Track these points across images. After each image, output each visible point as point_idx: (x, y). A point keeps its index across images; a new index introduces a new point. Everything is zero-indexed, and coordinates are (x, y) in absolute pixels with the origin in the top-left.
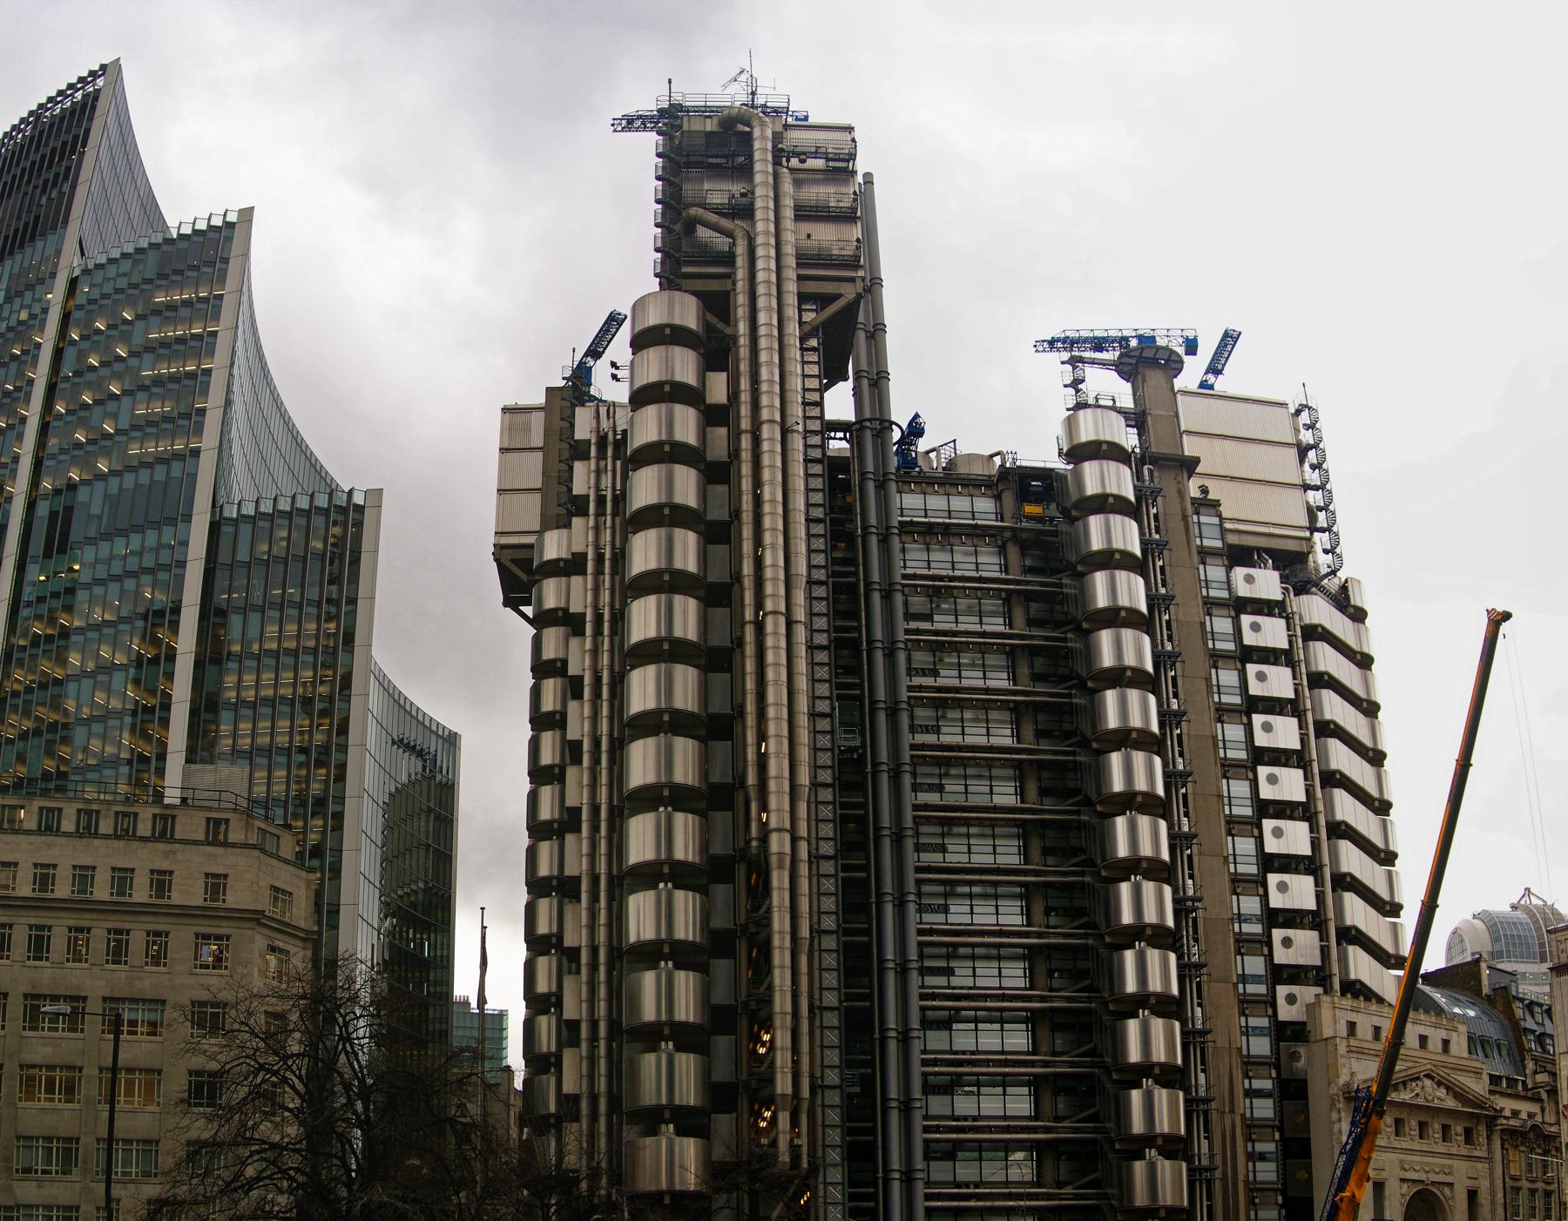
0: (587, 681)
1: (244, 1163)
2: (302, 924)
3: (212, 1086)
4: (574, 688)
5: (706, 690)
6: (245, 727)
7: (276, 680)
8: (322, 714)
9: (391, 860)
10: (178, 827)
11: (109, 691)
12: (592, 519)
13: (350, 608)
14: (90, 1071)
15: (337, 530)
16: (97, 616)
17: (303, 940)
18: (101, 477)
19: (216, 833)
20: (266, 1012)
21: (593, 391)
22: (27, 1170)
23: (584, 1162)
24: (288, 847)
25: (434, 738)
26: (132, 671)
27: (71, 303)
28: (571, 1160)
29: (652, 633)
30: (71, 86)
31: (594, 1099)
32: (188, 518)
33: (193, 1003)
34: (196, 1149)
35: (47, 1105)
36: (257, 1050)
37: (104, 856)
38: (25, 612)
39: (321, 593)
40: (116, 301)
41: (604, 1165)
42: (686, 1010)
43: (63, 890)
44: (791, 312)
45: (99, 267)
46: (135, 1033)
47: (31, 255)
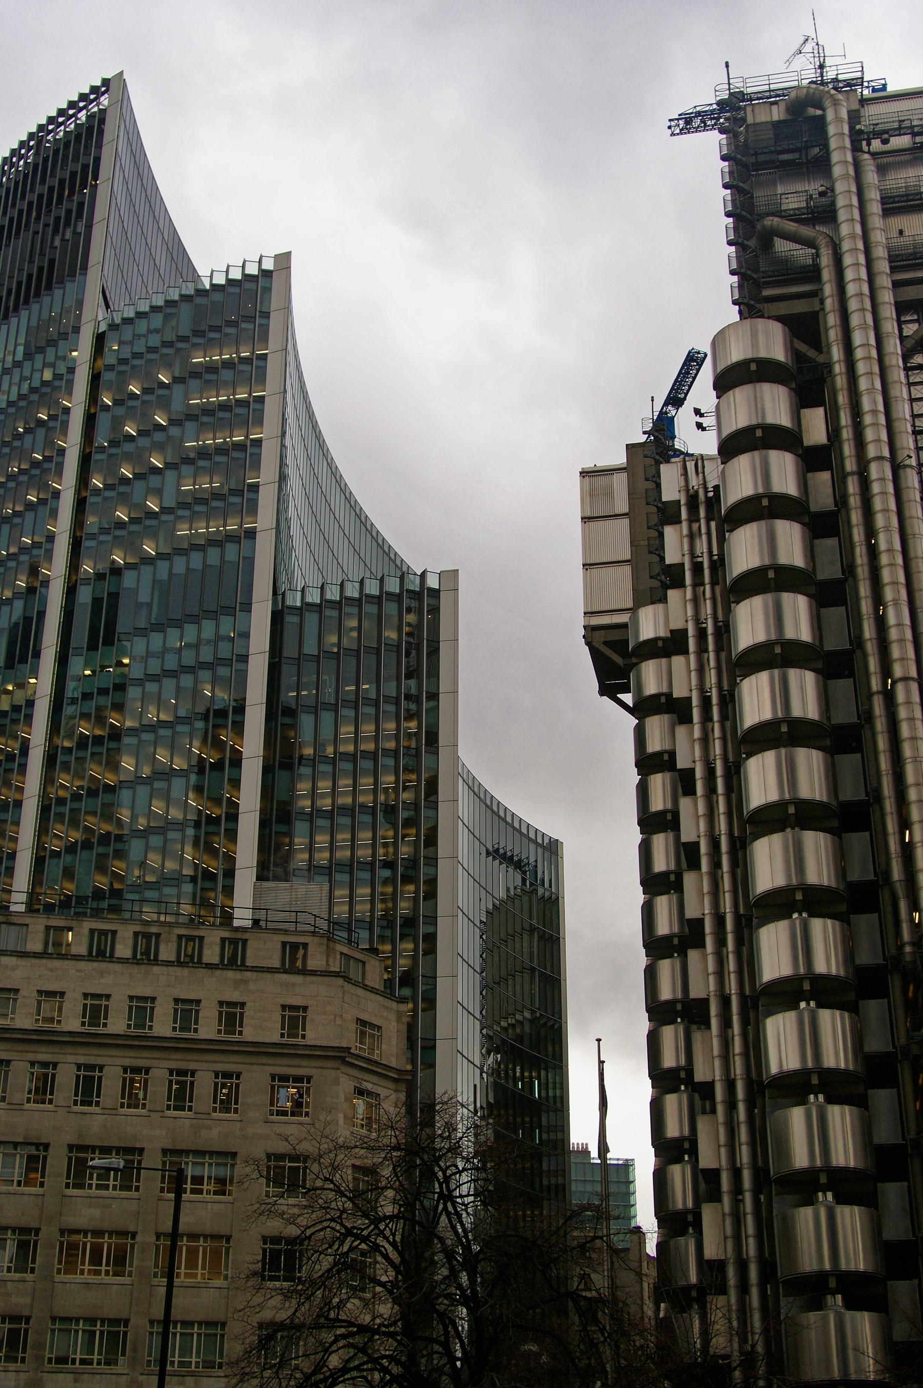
0: (699, 774)
1: (327, 1351)
2: (393, 1063)
3: (290, 1255)
4: (685, 783)
5: (834, 775)
6: (322, 839)
7: (355, 786)
8: (408, 823)
9: (492, 986)
10: (249, 952)
11: (168, 799)
12: (689, 590)
13: (432, 704)
14: (146, 1237)
15: (411, 618)
16: (151, 715)
17: (395, 1080)
18: (148, 560)
19: (293, 960)
20: (354, 1166)
22: (62, 1360)
23: (736, 1345)
24: (375, 974)
25: (532, 846)
26: (193, 778)
27: (100, 363)
28: (719, 1343)
29: (767, 715)
30: (72, 104)
31: (742, 1266)
32: (247, 607)
33: (269, 1156)
34: (270, 1334)
35: (92, 1279)
36: (344, 1211)
37: (165, 985)
38: (68, 710)
39: (399, 688)
40: (149, 361)
41: (760, 1349)
42: (845, 1152)
43: (117, 1023)
44: (890, 327)
45: (127, 321)
46: (200, 1192)
47: (51, 304)
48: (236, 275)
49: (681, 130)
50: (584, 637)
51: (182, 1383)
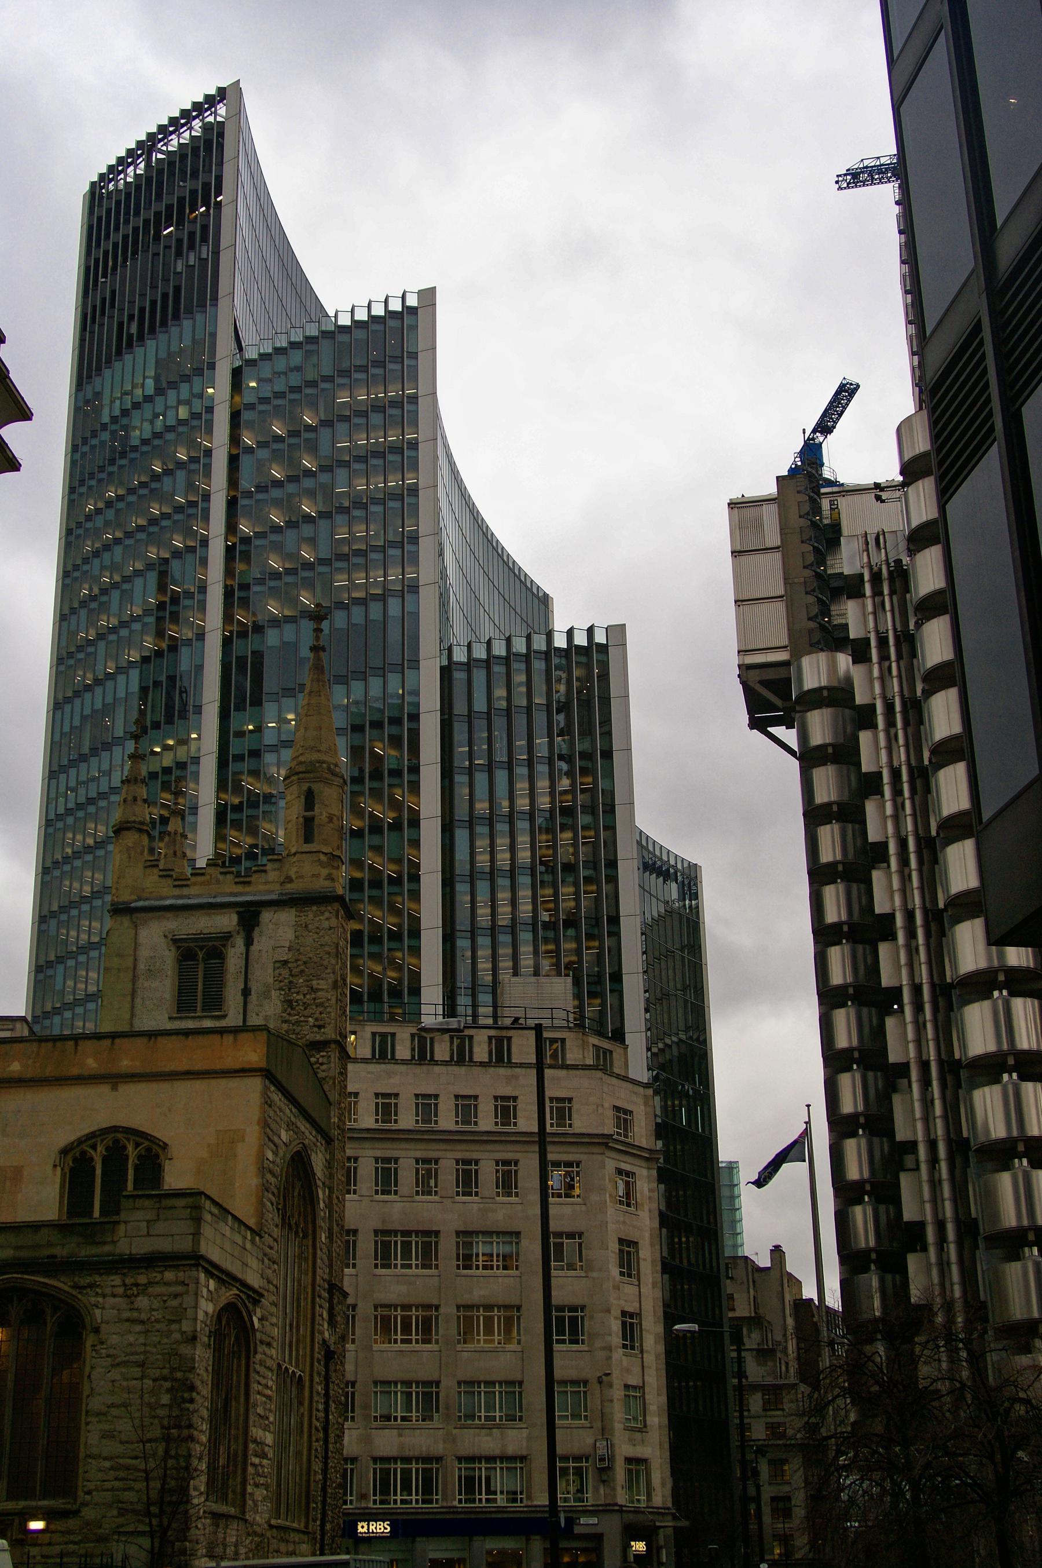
10: (514, 1049)
17: (647, 1159)
21: (827, 474)
32: (415, 664)
37: (446, 1082)
43: (407, 1119)
47: (181, 335)
48: (378, 310)
49: (848, 184)
50: (739, 676)
51: (491, 1435)
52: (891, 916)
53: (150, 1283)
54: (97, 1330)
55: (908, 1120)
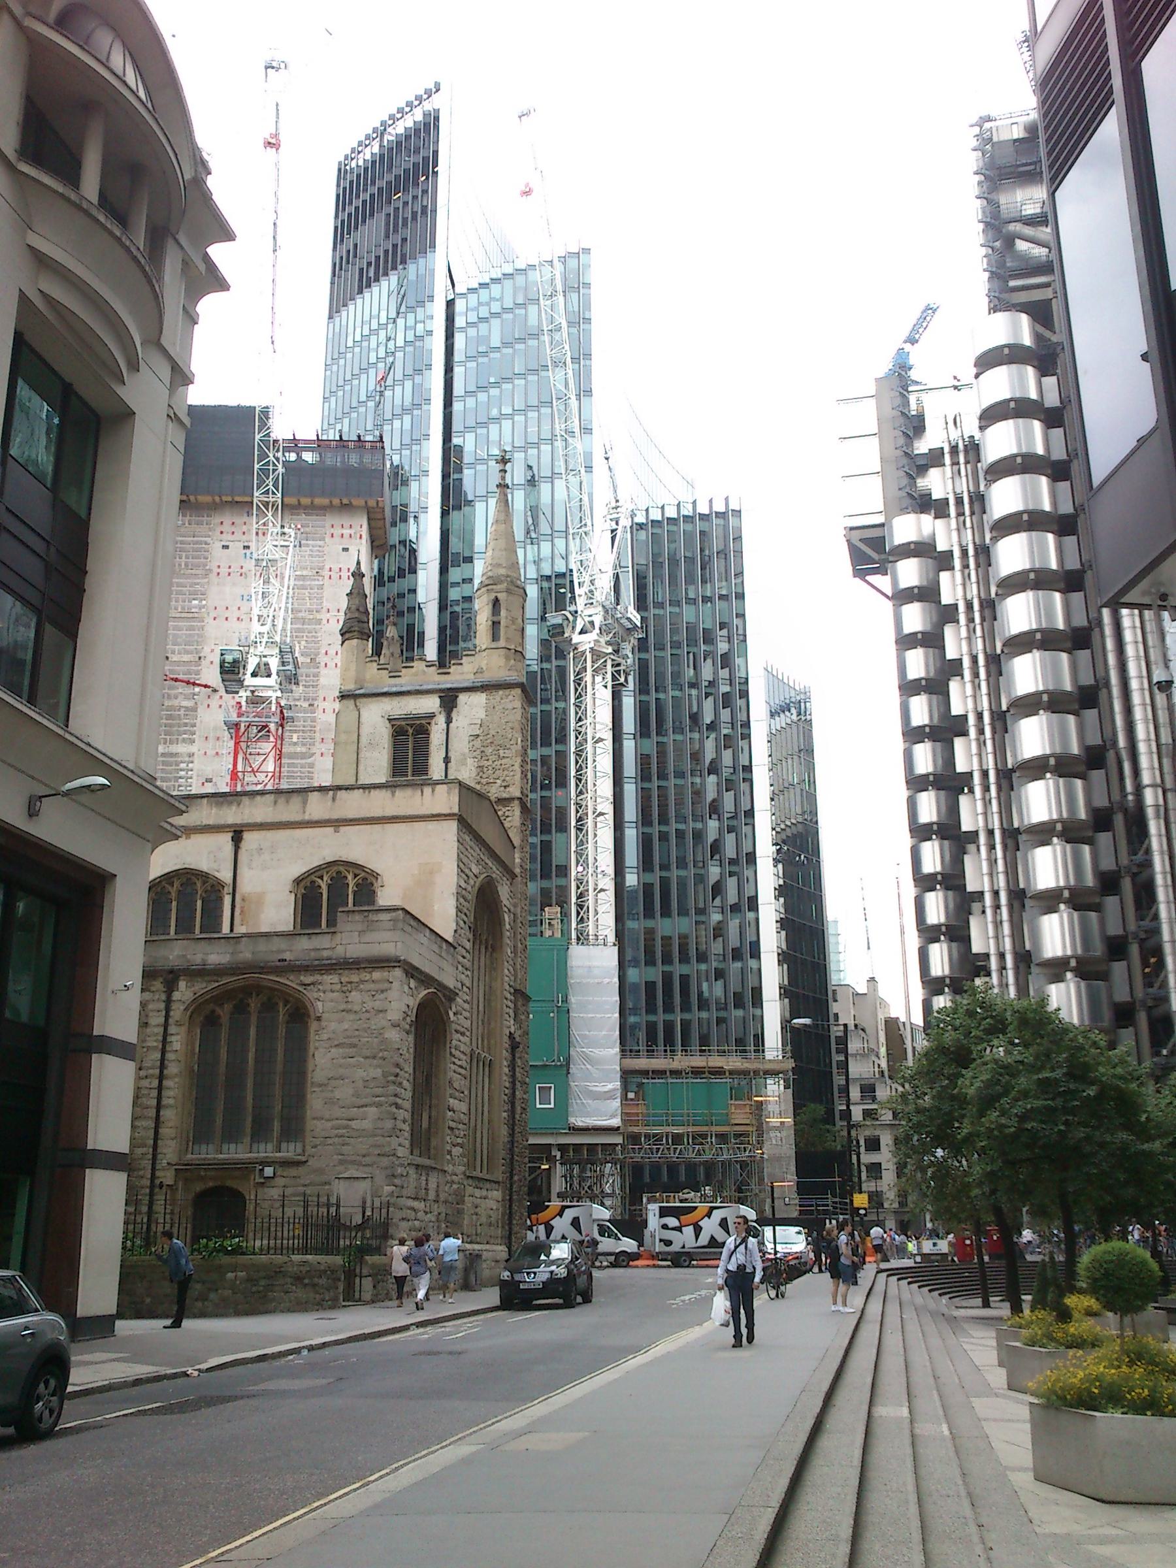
52: (965, 717)
53: (362, 982)
54: (319, 1019)
55: (978, 874)
